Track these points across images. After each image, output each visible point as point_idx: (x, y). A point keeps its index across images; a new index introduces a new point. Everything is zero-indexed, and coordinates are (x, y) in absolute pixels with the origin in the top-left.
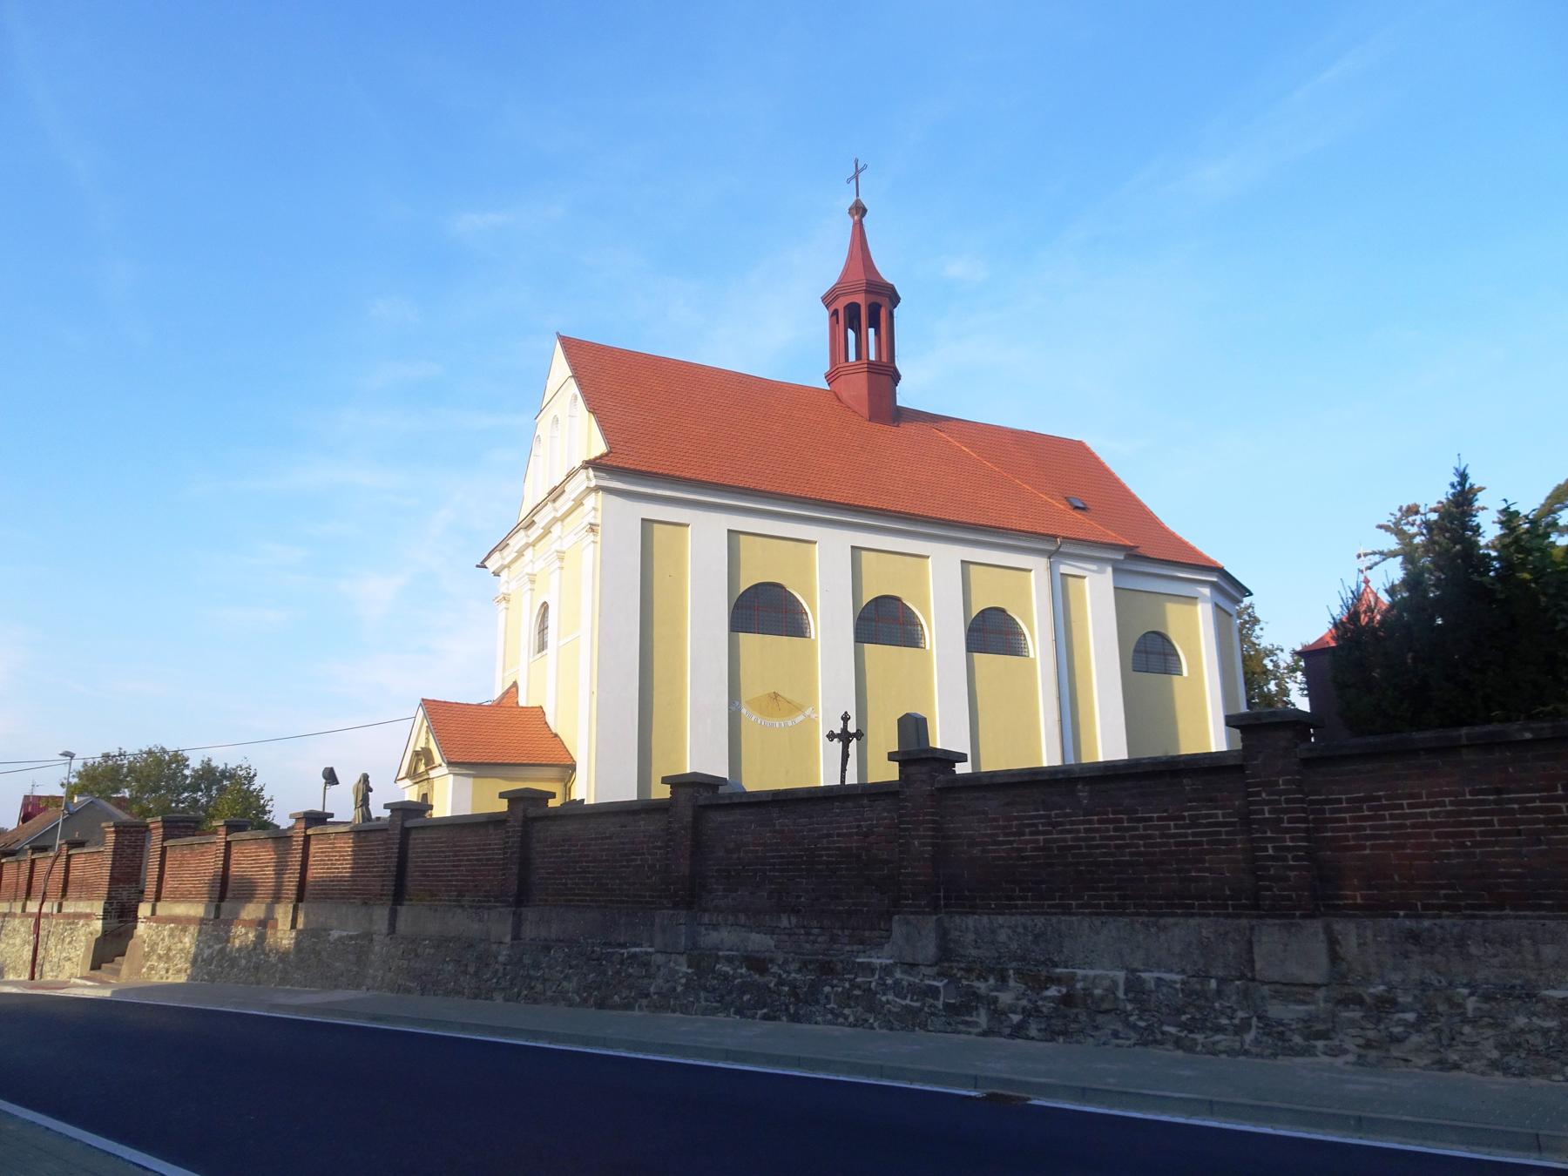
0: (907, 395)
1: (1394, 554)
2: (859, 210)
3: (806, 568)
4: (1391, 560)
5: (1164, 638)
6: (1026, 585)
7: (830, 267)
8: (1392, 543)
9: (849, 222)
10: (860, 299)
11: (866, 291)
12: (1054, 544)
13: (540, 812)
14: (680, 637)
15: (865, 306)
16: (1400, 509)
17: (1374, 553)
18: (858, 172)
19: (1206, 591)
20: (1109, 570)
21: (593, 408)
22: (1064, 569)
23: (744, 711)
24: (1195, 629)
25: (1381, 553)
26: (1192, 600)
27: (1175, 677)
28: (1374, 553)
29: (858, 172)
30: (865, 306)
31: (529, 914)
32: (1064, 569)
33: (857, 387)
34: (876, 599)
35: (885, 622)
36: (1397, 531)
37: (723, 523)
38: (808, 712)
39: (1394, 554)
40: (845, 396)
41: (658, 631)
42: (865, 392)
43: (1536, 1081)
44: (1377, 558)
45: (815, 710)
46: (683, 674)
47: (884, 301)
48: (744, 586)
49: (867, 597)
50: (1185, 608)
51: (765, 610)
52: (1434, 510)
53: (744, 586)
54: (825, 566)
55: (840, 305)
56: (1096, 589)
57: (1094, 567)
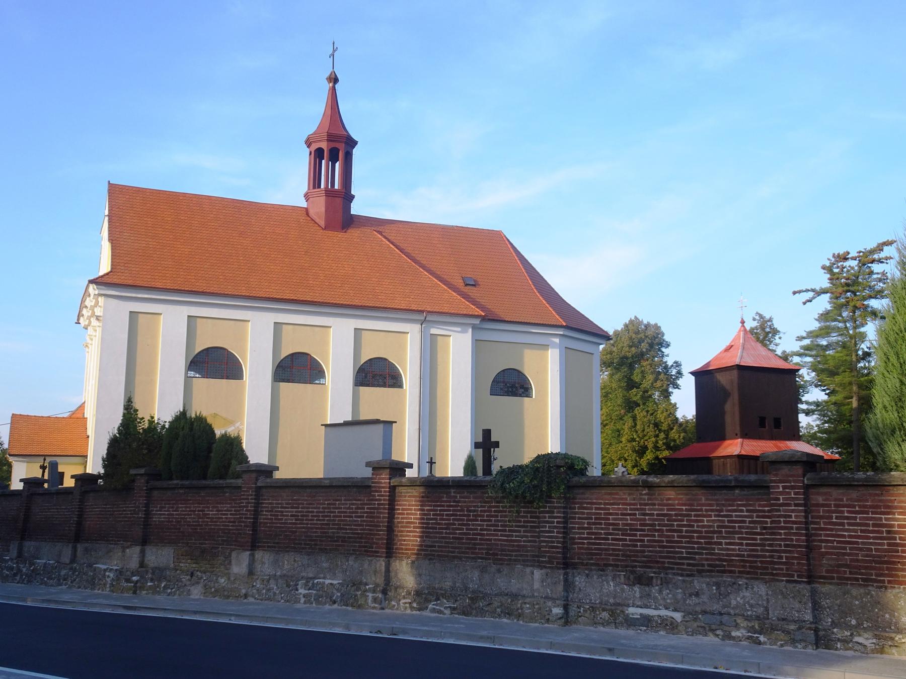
0: (357, 209)
1: (824, 291)
2: (334, 79)
3: (242, 338)
4: (823, 295)
5: (519, 374)
7: (311, 116)
9: (327, 86)
10: (324, 145)
12: (423, 314)
13: (583, 480)
14: (152, 382)
15: (334, 148)
16: (834, 256)
17: (807, 291)
18: (334, 51)
19: (557, 340)
22: (434, 331)
25: (813, 290)
26: (545, 347)
28: (807, 291)
29: (334, 51)
30: (334, 148)
31: (80, 547)
33: (319, 207)
34: (292, 355)
35: (296, 368)
36: (829, 269)
38: (237, 425)
39: (824, 291)
40: (311, 212)
41: (138, 379)
42: (323, 209)
43: (505, 620)
44: (811, 294)
45: (242, 424)
46: (154, 403)
47: (342, 147)
49: (285, 353)
50: (541, 352)
54: (337, 342)
55: (315, 146)
56: (458, 346)
57: (459, 329)
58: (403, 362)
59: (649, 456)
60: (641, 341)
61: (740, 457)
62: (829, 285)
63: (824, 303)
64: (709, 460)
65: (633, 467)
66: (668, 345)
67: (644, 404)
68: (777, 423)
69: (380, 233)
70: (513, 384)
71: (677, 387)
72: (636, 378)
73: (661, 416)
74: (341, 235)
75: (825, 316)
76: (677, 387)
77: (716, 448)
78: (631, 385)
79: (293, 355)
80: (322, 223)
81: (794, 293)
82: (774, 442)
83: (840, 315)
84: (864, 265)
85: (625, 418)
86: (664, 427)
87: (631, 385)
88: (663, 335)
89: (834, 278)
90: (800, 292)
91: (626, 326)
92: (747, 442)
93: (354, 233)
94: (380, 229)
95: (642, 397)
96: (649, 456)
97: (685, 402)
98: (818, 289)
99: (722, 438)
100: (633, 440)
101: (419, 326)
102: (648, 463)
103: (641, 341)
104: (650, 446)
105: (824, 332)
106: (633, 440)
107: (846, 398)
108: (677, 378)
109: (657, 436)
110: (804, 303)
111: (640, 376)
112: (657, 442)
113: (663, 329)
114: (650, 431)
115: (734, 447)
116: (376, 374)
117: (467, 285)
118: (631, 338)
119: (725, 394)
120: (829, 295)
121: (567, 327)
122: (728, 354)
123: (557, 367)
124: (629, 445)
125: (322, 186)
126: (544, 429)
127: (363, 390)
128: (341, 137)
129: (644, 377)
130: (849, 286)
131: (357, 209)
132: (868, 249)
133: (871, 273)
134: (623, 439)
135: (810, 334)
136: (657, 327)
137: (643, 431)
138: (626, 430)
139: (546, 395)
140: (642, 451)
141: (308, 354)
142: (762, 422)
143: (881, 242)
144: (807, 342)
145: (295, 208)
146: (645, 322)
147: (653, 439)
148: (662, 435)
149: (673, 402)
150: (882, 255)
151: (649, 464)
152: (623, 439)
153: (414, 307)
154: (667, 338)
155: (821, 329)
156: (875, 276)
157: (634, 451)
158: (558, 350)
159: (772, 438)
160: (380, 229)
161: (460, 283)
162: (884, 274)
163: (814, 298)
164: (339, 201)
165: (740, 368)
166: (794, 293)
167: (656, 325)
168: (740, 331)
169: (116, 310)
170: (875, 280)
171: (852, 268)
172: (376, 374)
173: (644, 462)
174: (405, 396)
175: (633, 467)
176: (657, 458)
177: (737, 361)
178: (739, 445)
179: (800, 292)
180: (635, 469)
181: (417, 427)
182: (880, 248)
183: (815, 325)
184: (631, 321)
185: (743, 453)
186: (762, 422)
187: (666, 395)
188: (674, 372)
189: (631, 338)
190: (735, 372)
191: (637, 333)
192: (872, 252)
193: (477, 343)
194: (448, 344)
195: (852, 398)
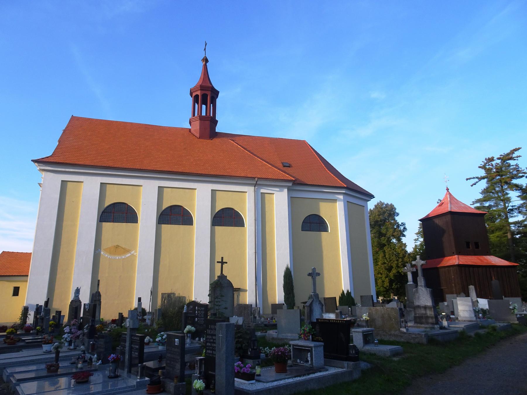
0: (219, 129)
1: (483, 178)
2: (206, 60)
3: (192, 199)
4: (482, 180)
6: (244, 199)
8: (482, 173)
9: (202, 64)
10: (199, 93)
11: (201, 90)
12: (256, 181)
16: (486, 159)
17: (474, 178)
19: (341, 197)
20: (286, 190)
21: (61, 141)
22: (263, 191)
23: (102, 253)
24: (336, 211)
25: (477, 178)
26: (335, 201)
27: (323, 234)
28: (474, 178)
29: (205, 49)
30: (206, 95)
32: (263, 191)
33: (196, 127)
34: (223, 209)
35: (174, 215)
36: (483, 167)
37: (156, 184)
38: (132, 252)
39: (483, 178)
40: (192, 131)
41: (66, 223)
42: (198, 127)
45: (136, 252)
48: (107, 203)
50: (330, 204)
51: (118, 213)
52: (498, 159)
53: (217, 210)
54: (200, 198)
55: (194, 94)
58: (244, 209)
59: (394, 271)
60: (384, 212)
61: (459, 265)
62: (485, 175)
63: (483, 184)
64: (437, 269)
65: (386, 277)
66: (398, 214)
67: (388, 245)
68: (477, 245)
69: (233, 141)
70: (315, 224)
71: (404, 236)
72: (383, 231)
73: (399, 251)
74: (208, 141)
75: (485, 191)
76: (404, 236)
77: (440, 262)
78: (381, 235)
79: (171, 207)
80: (198, 135)
81: (467, 179)
82: (476, 257)
83: (495, 190)
84: (504, 162)
85: (379, 252)
86: (401, 255)
87: (381, 235)
88: (395, 209)
89: (488, 171)
90: (470, 179)
91: (376, 206)
92: (461, 257)
93: (216, 141)
94: (233, 139)
95: (387, 241)
96: (394, 271)
97: (412, 240)
98: (479, 177)
99: (443, 256)
100: (384, 263)
101: (253, 188)
102: (394, 275)
103: (384, 212)
104: (394, 265)
105: (485, 200)
106: (384, 263)
107: (504, 233)
108: (404, 231)
109: (397, 261)
110: (472, 186)
111: (385, 230)
112: (398, 264)
113: (395, 206)
114: (394, 258)
115: (454, 260)
116: (226, 218)
117: (284, 166)
118: (379, 211)
119: (441, 232)
120: (486, 180)
121: (347, 188)
122: (442, 207)
123: (343, 213)
124: (383, 266)
125: (196, 114)
126: (339, 276)
127: (218, 228)
128: (209, 87)
129: (387, 231)
130: (499, 174)
131: (218, 129)
132: (506, 153)
133: (509, 165)
134: (379, 263)
135: (478, 201)
136: (392, 206)
137: (390, 258)
138: (381, 258)
139: (337, 230)
140: (390, 269)
141: (181, 206)
142: (468, 244)
143: (512, 149)
144: (478, 205)
145: (183, 129)
146: (386, 203)
147: (396, 262)
148: (400, 260)
149: (404, 242)
150: (514, 155)
151: (395, 276)
152: (379, 263)
153: (249, 175)
154: (397, 211)
155: (484, 197)
156: (512, 167)
157: (386, 269)
158: (343, 203)
159: (475, 254)
160: (233, 139)
161: (281, 166)
162: (517, 165)
163: (477, 182)
164: (208, 123)
165: (451, 213)
166: (467, 179)
167: (391, 204)
168: (446, 194)
169: (54, 180)
170: (512, 169)
171: (498, 164)
172: (226, 218)
173: (391, 274)
174: (245, 231)
175: (386, 277)
176: (398, 272)
177: (449, 210)
178: (457, 259)
179: (470, 179)
180: (387, 279)
181: (254, 251)
182: (513, 152)
183: (480, 196)
184: (378, 204)
185: (461, 263)
186: (468, 244)
187: (399, 240)
188: (402, 228)
189: (379, 211)
190: (449, 217)
191: (382, 208)
192: (508, 154)
193: (292, 201)
194: (272, 200)
195: (507, 233)
